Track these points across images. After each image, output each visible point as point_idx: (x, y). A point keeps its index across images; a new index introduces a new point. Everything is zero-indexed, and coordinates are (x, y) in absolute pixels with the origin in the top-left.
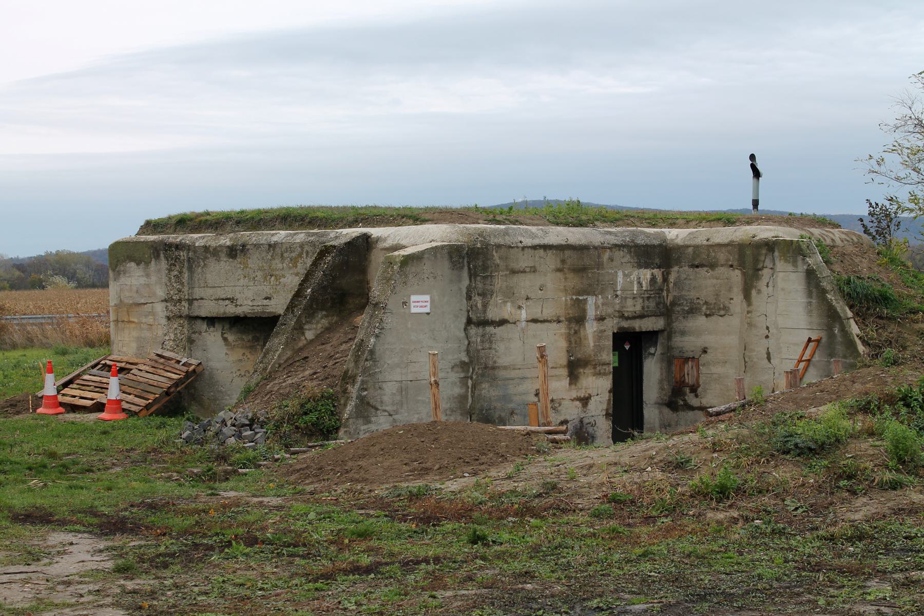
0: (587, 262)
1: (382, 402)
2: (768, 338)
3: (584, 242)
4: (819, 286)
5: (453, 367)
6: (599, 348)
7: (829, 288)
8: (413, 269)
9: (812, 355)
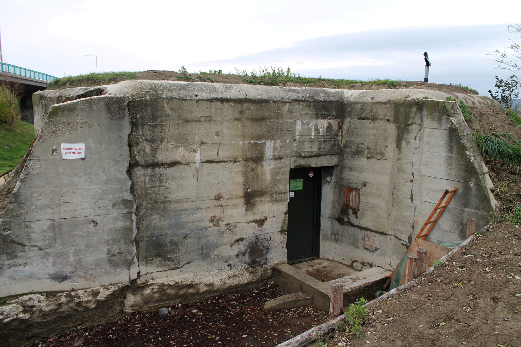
0: (265, 112)
1: (30, 239)
2: (414, 182)
3: (264, 96)
4: (460, 143)
5: (114, 205)
6: (275, 181)
7: (468, 145)
8: (64, 120)
9: (448, 203)
